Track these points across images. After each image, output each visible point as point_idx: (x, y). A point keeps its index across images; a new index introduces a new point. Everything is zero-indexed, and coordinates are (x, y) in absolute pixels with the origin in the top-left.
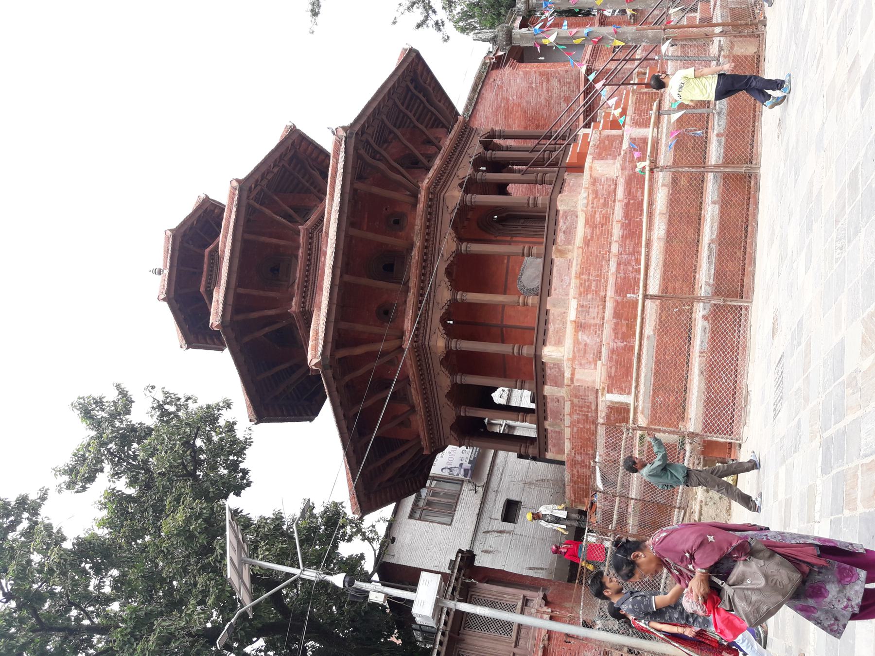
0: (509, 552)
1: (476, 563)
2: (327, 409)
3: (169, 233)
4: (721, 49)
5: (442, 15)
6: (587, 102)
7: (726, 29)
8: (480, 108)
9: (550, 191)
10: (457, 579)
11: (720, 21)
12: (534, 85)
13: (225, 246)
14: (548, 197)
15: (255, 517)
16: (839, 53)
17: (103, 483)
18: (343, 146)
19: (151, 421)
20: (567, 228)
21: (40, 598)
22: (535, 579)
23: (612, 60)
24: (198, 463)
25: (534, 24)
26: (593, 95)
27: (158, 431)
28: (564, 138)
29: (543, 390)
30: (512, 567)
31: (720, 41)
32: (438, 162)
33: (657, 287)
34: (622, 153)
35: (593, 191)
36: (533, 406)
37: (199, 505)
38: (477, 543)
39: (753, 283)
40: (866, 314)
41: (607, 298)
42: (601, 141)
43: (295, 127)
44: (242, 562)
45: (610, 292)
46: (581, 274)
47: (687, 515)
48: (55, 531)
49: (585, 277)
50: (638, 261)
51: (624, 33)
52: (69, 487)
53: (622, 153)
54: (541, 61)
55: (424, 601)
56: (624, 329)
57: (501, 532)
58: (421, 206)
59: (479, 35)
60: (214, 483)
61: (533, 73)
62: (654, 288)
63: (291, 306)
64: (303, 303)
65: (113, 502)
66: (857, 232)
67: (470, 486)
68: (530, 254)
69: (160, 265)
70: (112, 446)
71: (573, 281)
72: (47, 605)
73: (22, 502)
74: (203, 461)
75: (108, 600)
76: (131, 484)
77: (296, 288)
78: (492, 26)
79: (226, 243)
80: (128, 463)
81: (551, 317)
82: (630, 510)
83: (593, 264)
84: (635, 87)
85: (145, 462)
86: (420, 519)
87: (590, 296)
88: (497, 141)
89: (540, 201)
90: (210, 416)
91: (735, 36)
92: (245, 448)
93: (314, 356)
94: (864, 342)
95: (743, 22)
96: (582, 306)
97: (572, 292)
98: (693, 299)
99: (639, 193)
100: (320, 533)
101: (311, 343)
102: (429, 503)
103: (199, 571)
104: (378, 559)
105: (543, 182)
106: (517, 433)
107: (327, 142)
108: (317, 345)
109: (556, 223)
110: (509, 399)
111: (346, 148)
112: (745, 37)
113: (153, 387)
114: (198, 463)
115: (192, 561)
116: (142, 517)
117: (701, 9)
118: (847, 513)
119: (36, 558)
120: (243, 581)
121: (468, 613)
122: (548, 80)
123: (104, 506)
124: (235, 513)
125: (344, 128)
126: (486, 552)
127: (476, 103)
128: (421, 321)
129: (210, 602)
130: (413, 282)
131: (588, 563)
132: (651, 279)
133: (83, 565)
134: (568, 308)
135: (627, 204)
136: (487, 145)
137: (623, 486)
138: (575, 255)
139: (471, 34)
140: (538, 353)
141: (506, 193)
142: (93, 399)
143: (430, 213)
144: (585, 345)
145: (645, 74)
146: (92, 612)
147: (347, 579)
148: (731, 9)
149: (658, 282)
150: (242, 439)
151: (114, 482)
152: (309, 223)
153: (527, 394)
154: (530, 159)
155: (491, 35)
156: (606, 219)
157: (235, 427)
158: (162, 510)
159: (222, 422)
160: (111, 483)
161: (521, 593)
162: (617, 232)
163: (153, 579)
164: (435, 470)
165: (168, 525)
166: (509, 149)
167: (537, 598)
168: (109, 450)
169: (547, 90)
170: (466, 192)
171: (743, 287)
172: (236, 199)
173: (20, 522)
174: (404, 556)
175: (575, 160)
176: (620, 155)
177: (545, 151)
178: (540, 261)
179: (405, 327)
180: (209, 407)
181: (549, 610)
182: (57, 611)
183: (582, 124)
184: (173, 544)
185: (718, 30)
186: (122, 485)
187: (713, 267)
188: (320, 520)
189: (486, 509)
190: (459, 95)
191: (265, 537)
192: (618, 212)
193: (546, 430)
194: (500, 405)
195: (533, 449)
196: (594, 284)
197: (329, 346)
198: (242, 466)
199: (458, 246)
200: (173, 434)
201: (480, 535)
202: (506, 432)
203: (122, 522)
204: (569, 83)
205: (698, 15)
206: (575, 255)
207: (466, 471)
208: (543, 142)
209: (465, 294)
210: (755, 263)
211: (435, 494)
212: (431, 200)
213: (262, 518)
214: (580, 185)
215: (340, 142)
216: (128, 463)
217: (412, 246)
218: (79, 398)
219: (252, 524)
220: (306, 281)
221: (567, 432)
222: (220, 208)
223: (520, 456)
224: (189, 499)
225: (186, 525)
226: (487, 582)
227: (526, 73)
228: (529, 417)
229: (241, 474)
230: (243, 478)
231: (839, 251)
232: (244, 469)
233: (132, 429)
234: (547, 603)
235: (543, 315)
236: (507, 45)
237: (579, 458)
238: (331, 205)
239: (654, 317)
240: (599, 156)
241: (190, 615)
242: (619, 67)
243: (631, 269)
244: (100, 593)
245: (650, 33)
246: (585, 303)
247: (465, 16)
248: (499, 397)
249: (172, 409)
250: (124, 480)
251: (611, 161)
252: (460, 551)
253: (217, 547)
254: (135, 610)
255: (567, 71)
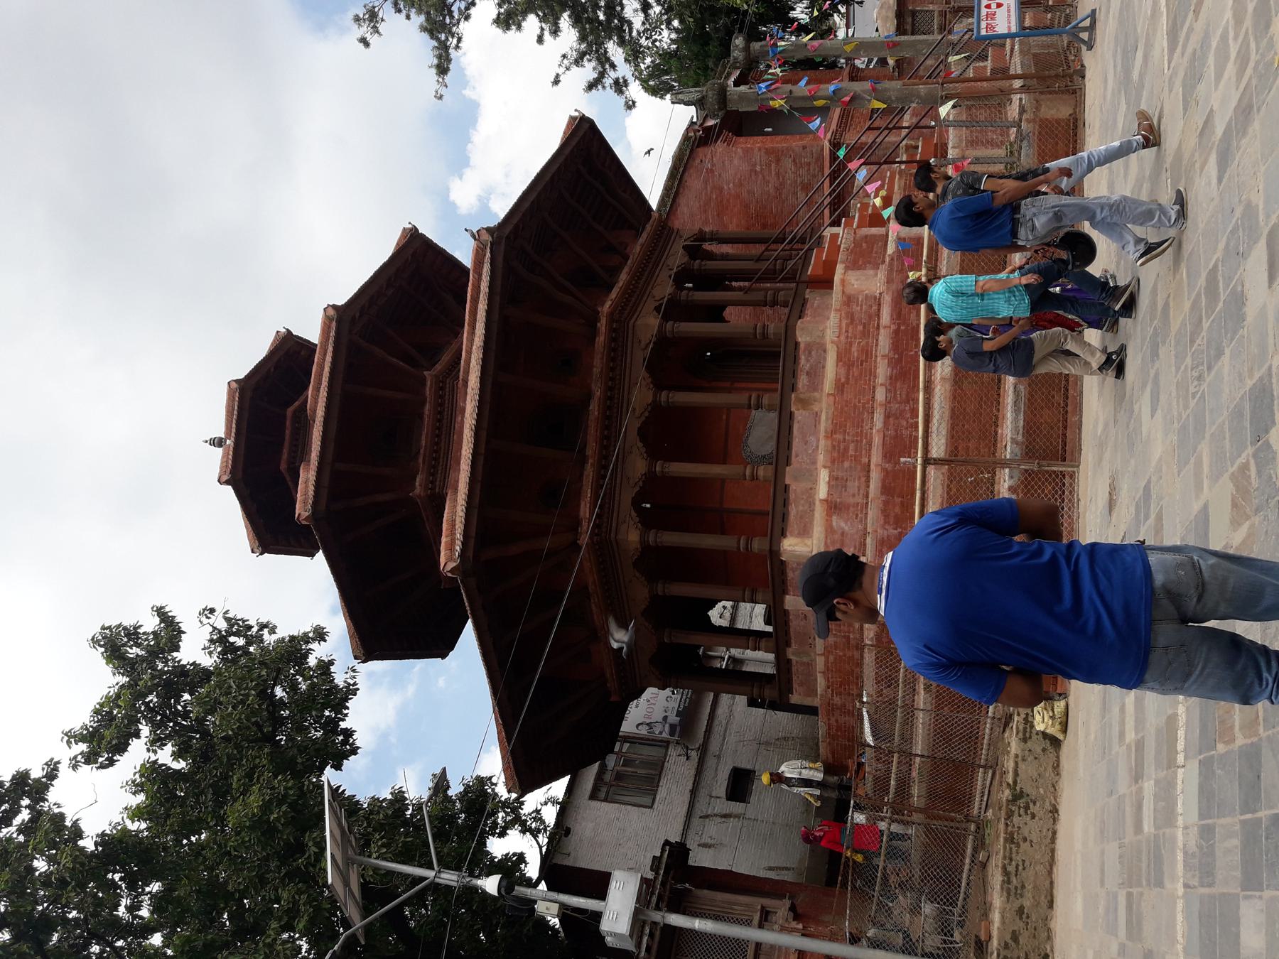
0: (738, 845)
1: (690, 862)
2: (469, 630)
3: (234, 385)
4: (1022, 110)
5: (624, 70)
6: (834, 190)
7: (1029, 82)
8: (682, 201)
9: (784, 318)
10: (663, 884)
11: (1019, 71)
12: (758, 168)
13: (316, 403)
14: (783, 325)
15: (363, 797)
16: (1185, 109)
17: (137, 753)
18: (488, 255)
19: (207, 661)
20: (811, 368)
21: (47, 924)
22: (778, 881)
23: (869, 129)
24: (278, 722)
25: (759, 80)
26: (843, 179)
27: (220, 674)
28: (803, 240)
29: (783, 602)
30: (743, 867)
31: (1021, 99)
32: (624, 277)
33: (943, 448)
34: (887, 259)
35: (847, 313)
36: (770, 629)
37: (283, 783)
38: (691, 835)
39: (1080, 439)
40: (1236, 466)
41: (872, 467)
42: (857, 243)
43: (417, 230)
44: (348, 862)
45: (876, 457)
46: (833, 432)
47: (997, 777)
48: (68, 823)
49: (839, 436)
50: (914, 413)
51: (886, 90)
52: (88, 762)
53: (887, 259)
54: (768, 134)
55: (617, 913)
56: (897, 510)
57: (726, 816)
58: (601, 340)
59: (680, 96)
60: (302, 749)
61: (756, 151)
62: (938, 448)
63: (414, 488)
64: (432, 482)
65: (154, 782)
66: (1220, 353)
67: (680, 750)
68: (758, 406)
69: (221, 433)
70: (152, 698)
71: (822, 443)
72: (55, 937)
73: (21, 779)
74: (286, 718)
75: (147, 930)
76: (177, 756)
77: (421, 460)
78: (696, 85)
79: (318, 399)
80: (176, 724)
81: (792, 496)
82: (915, 774)
83: (850, 417)
84: (903, 167)
85: (201, 721)
86: (605, 800)
87: (846, 464)
88: (707, 246)
89: (771, 330)
90: (295, 650)
91: (1041, 93)
92: (347, 700)
93: (448, 559)
94: (1235, 505)
95: (1053, 73)
96: (837, 479)
97: (821, 458)
98: (995, 463)
99: (913, 316)
100: (463, 818)
101: (444, 540)
102: (619, 777)
103: (282, 880)
104: (545, 859)
105: (774, 303)
106: (748, 668)
107: (463, 252)
108: (453, 542)
109: (796, 360)
110: (733, 618)
111: (492, 259)
112: (1056, 93)
113: (212, 611)
114: (278, 722)
115: (273, 865)
116: (197, 802)
117: (993, 56)
118: (1221, 748)
119: (41, 865)
120: (350, 890)
121: (681, 929)
122: (778, 161)
123: (137, 788)
124: (335, 792)
125: (489, 230)
126: (705, 845)
127: (677, 194)
128: (605, 504)
129: (301, 926)
130: (592, 449)
131: (856, 851)
132: (934, 435)
133: (110, 876)
134: (815, 482)
135: (897, 332)
136: (694, 251)
137: (902, 737)
138: (824, 407)
139: (668, 97)
140: (775, 548)
141: (724, 321)
142: (125, 628)
143: (614, 350)
144: (843, 534)
145: (917, 147)
146: (122, 948)
147: (504, 883)
148: (1035, 55)
149: (943, 441)
150: (342, 685)
151: (155, 752)
152: (438, 367)
153: (760, 609)
154: (756, 272)
155: (696, 96)
156: (867, 353)
157: (333, 669)
158: (227, 792)
159: (312, 661)
160: (151, 754)
161: (758, 902)
162: (882, 371)
163: (215, 896)
164: (628, 727)
165: (236, 813)
166: (725, 257)
167: (781, 909)
168: (147, 704)
169: (778, 174)
170: (666, 318)
171: (1065, 444)
172: (333, 334)
173: (18, 812)
174: (583, 857)
175: (820, 272)
176: (884, 262)
177: (776, 260)
178: (774, 415)
179: (582, 514)
180: (292, 638)
181: (800, 926)
182: (71, 946)
183: (827, 221)
184: (243, 842)
185: (1017, 83)
186: (165, 756)
187: (1021, 417)
188: (458, 805)
189: (703, 784)
190: (651, 181)
191: (380, 827)
192: (884, 342)
193: (789, 661)
194: (720, 627)
195: (771, 692)
196: (852, 446)
197: (472, 543)
198: (343, 725)
199: (655, 396)
200: (243, 679)
201: (695, 821)
202: (731, 667)
203: (167, 810)
204: (809, 164)
205: (989, 64)
206: (824, 405)
207: (673, 727)
208: (773, 246)
209: (666, 465)
210: (1081, 410)
211: (627, 763)
212: (615, 330)
213: (374, 800)
214: (828, 307)
215: (484, 250)
216: (176, 724)
217: (589, 396)
218: (103, 628)
219: (361, 809)
220: (436, 452)
221: (820, 663)
222: (307, 347)
223: (752, 703)
224: (268, 775)
225: (264, 813)
226: (709, 888)
227: (746, 151)
228: (763, 643)
229: (341, 738)
230: (345, 742)
231: (1196, 383)
232: (346, 729)
233: (181, 671)
234: (797, 917)
235: (781, 494)
236: (720, 109)
237: (837, 700)
238: (471, 341)
239: (939, 491)
240: (853, 265)
241: (270, 946)
242: (879, 140)
243: (904, 423)
244: (135, 917)
245: (922, 89)
246: (840, 474)
247: (656, 71)
248: (718, 615)
249: (240, 642)
250: (169, 748)
251: (871, 272)
252: (667, 843)
253: (310, 844)
254: (188, 940)
255: (804, 148)
